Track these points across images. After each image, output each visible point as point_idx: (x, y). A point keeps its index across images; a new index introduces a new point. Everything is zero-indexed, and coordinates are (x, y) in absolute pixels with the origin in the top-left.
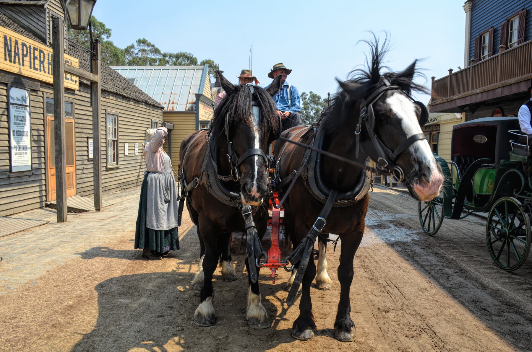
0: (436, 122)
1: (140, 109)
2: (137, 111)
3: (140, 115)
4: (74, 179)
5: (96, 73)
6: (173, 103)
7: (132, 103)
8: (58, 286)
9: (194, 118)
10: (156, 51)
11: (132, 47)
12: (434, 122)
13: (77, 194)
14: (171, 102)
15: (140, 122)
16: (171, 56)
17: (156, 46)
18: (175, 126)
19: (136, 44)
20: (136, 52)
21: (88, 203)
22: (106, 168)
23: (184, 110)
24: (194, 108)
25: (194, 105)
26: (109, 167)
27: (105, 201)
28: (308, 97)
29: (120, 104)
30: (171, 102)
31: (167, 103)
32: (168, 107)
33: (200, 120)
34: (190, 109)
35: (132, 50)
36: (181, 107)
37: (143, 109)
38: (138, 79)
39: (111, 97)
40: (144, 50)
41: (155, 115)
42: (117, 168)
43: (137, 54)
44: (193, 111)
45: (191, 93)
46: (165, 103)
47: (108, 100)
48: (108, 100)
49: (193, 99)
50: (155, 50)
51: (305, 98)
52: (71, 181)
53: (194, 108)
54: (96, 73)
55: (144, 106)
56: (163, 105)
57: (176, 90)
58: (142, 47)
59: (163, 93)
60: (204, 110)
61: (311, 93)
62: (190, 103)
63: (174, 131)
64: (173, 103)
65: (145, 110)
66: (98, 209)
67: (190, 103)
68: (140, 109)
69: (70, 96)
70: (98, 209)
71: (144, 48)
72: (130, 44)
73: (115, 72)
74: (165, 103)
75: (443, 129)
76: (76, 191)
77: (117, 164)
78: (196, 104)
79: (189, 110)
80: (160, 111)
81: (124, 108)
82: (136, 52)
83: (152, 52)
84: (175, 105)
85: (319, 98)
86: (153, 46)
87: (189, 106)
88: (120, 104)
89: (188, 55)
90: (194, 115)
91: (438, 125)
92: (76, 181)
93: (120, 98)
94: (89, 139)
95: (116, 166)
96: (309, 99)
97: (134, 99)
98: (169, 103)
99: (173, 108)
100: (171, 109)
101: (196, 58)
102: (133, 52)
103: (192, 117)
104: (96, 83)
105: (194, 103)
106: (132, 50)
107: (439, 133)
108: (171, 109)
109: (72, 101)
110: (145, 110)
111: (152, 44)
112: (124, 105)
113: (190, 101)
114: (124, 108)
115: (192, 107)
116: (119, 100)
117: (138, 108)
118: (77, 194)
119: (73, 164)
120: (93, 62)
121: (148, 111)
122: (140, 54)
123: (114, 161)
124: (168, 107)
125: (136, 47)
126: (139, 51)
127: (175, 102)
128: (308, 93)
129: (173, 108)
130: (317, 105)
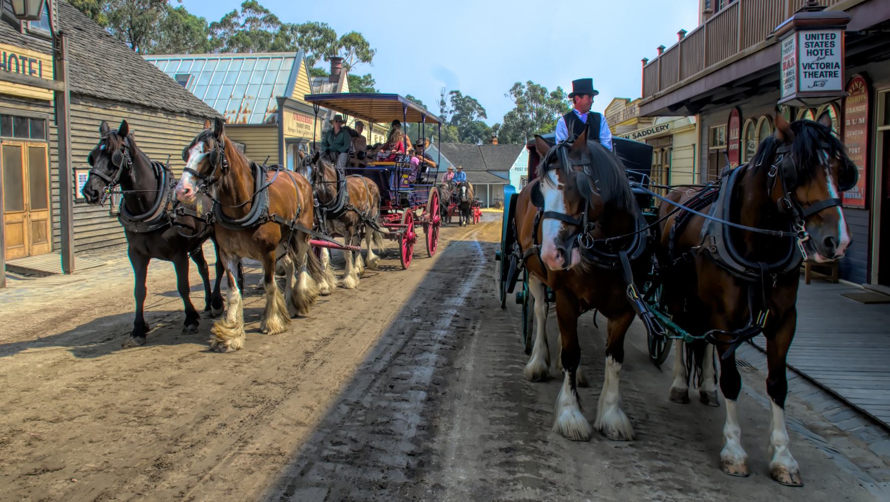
0: (665, 131)
1: (179, 123)
2: (173, 127)
3: (177, 133)
4: (49, 228)
5: (62, 79)
6: (245, 112)
7: (162, 115)
8: (560, 472)
9: (277, 134)
10: (272, 19)
11: (234, 14)
12: (663, 131)
13: (53, 250)
14: (242, 110)
15: (178, 142)
16: (293, 29)
19: (239, 9)
21: (53, 261)
22: (111, 213)
23: (260, 122)
24: (276, 119)
25: (277, 115)
27: (78, 262)
28: (524, 90)
29: (137, 117)
30: (242, 110)
31: (237, 111)
32: (237, 117)
33: (285, 137)
34: (270, 120)
35: (234, 20)
37: (182, 124)
38: (194, 74)
39: (119, 108)
40: (254, 20)
43: (244, 26)
44: (275, 124)
45: (274, 96)
46: (234, 112)
47: (114, 113)
48: (114, 113)
49: (274, 105)
51: (520, 93)
52: (44, 232)
53: (276, 119)
54: (62, 79)
55: (185, 119)
57: (252, 92)
58: (249, 14)
60: (295, 122)
61: (530, 83)
64: (245, 112)
65: (188, 124)
66: (67, 269)
68: (179, 123)
69: (41, 109)
70: (67, 269)
72: (229, 11)
73: (150, 66)
74: (234, 112)
75: (678, 142)
76: (53, 246)
78: (279, 112)
81: (147, 124)
82: (241, 21)
83: (266, 22)
84: (248, 115)
85: (543, 91)
86: (266, 11)
87: (268, 115)
88: (137, 117)
90: (277, 130)
91: (670, 137)
92: (52, 233)
93: (137, 109)
94: (77, 171)
96: (526, 94)
97: (163, 109)
99: (244, 119)
100: (242, 121)
101: (333, 31)
103: (274, 133)
104: (62, 93)
105: (276, 112)
107: (671, 149)
108: (242, 121)
109: (44, 117)
110: (188, 124)
111: (265, 8)
112: (146, 118)
113: (271, 108)
114: (147, 124)
115: (273, 118)
116: (135, 111)
117: (173, 122)
118: (53, 250)
119: (46, 207)
120: (57, 63)
121: (193, 125)
122: (248, 25)
124: (237, 117)
125: (240, 14)
126: (247, 21)
128: (524, 83)
129: (244, 119)
130: (540, 103)
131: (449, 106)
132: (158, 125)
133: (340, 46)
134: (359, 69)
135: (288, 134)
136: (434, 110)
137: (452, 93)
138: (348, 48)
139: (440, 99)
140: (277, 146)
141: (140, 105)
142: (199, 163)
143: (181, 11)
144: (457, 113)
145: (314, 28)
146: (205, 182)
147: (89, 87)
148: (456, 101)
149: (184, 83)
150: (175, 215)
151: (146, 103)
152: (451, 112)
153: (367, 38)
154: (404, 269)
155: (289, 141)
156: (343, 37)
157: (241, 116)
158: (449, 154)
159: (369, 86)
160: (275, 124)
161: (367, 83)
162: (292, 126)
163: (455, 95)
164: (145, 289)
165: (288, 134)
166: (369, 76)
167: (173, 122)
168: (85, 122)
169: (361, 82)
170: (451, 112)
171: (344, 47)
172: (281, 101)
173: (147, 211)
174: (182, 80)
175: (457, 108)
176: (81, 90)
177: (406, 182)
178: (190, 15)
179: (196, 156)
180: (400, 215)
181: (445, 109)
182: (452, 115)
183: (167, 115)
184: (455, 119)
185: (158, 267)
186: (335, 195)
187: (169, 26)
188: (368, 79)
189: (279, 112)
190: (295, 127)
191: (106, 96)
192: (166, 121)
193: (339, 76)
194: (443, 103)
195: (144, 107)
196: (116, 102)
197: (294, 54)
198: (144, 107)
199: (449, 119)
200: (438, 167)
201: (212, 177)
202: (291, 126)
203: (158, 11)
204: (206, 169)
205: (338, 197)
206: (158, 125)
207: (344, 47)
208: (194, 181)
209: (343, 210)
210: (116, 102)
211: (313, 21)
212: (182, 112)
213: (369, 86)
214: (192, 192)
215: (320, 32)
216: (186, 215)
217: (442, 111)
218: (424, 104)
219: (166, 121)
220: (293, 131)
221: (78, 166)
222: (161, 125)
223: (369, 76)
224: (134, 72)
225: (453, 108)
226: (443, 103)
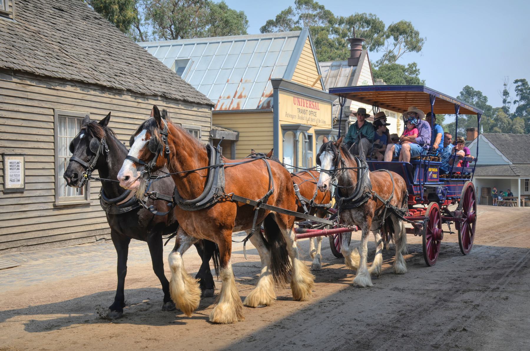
7: (129, 98)
11: (289, 11)
14: (237, 95)
16: (341, 22)
17: (326, 8)
18: (241, 134)
20: (295, 19)
23: (255, 107)
24: (272, 104)
26: (60, 203)
30: (237, 95)
31: (232, 97)
33: (280, 123)
34: (265, 105)
35: (289, 17)
36: (250, 103)
38: (194, 59)
40: (307, 16)
41: (191, 117)
42: (88, 205)
43: (298, 22)
44: (270, 109)
46: (228, 97)
50: (325, 15)
53: (272, 104)
56: (214, 102)
59: (228, 81)
60: (296, 107)
62: (266, 96)
63: (239, 143)
64: (240, 97)
67: (266, 96)
71: (307, 12)
72: (285, 8)
74: (228, 97)
77: (86, 199)
78: (274, 96)
79: (263, 108)
80: (207, 110)
83: (321, 18)
84: (243, 100)
86: (322, 8)
87: (264, 99)
89: (369, 18)
90: (271, 116)
93: (95, 90)
95: (85, 202)
97: (129, 91)
98: (234, 97)
99: (238, 104)
101: (381, 22)
102: (290, 20)
103: (268, 120)
105: (271, 96)
106: (289, 17)
111: (320, 4)
115: (269, 103)
123: (81, 193)
125: (295, 11)
127: (243, 95)
129: (238, 104)
131: (513, 96)
132: (123, 109)
133: (388, 37)
134: (405, 59)
135: (284, 119)
136: (495, 101)
137: (516, 81)
138: (396, 39)
139: (503, 89)
140: (272, 134)
141: (96, 85)
142: (141, 151)
143: (222, 7)
144: (522, 103)
145: (362, 18)
146: (147, 168)
147: (28, 64)
148: (521, 90)
149: (181, 70)
150: (146, 199)
151: (105, 84)
152: (515, 102)
153: (416, 27)
154: (428, 265)
155: (286, 128)
156: (390, 27)
157: (236, 101)
158: (501, 145)
159: (414, 76)
160: (270, 109)
161: (412, 72)
162: (289, 110)
163: (520, 83)
164: (126, 267)
165: (284, 119)
166: (414, 64)
167: (143, 106)
168: (19, 101)
169: (404, 70)
170: (515, 102)
171: (392, 37)
172: (277, 84)
173: (121, 195)
174: (182, 65)
175: (522, 98)
176: (12, 66)
177: (435, 176)
178: (230, 10)
179: (140, 142)
180: (425, 209)
181: (508, 100)
182: (517, 105)
183: (136, 98)
184: (520, 110)
185: (137, 246)
186: (355, 184)
187: (212, 20)
188: (413, 68)
189: (274, 96)
190: (295, 113)
191: (47, 73)
192: (135, 104)
193: (359, 58)
194: (506, 93)
195: (103, 88)
196: (63, 81)
197: (297, 33)
198: (103, 88)
199: (513, 109)
200: (476, 160)
201: (153, 163)
202: (289, 112)
203: (200, 7)
204: (147, 156)
205: (357, 185)
206: (123, 109)
207: (392, 37)
208: (135, 168)
209: (362, 198)
210: (63, 81)
211: (360, 13)
212: (155, 96)
213: (414, 76)
214: (132, 179)
215: (368, 22)
216: (158, 199)
217: (504, 101)
218: (484, 94)
219: (135, 104)
220: (292, 117)
221: (7, 151)
222: (127, 109)
223: (414, 64)
224: (109, 54)
225: (518, 98)
226: (506, 93)
